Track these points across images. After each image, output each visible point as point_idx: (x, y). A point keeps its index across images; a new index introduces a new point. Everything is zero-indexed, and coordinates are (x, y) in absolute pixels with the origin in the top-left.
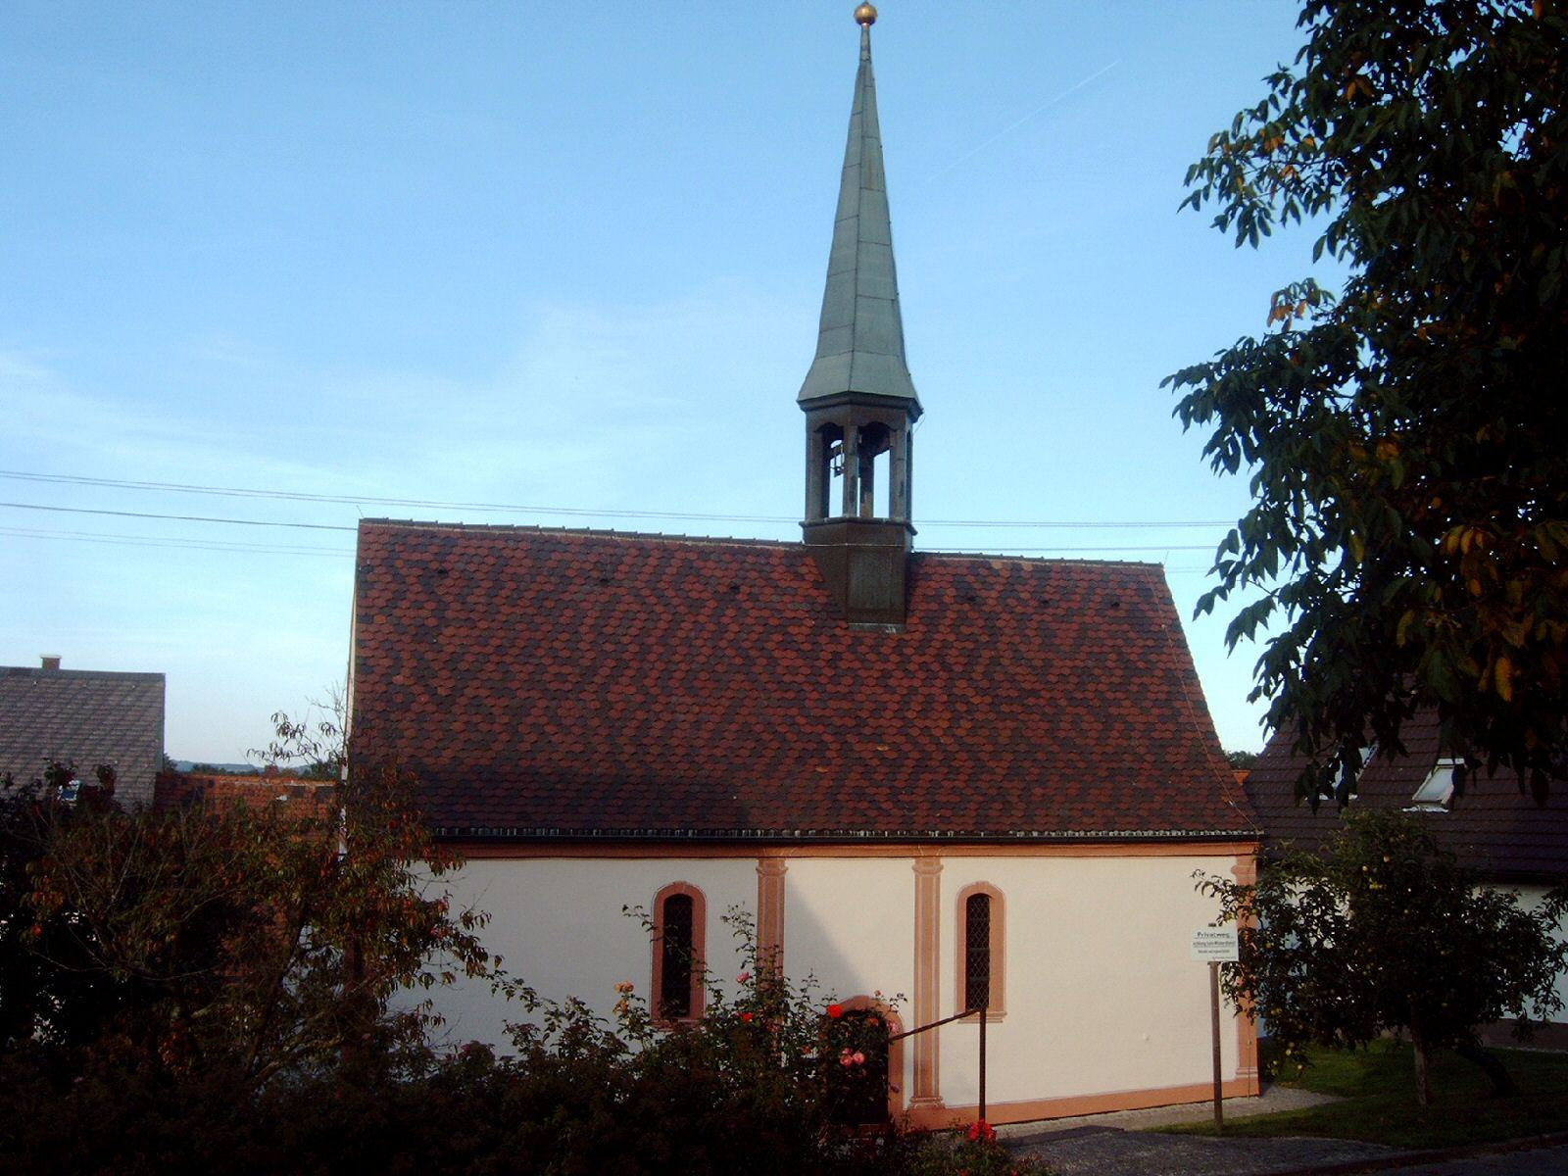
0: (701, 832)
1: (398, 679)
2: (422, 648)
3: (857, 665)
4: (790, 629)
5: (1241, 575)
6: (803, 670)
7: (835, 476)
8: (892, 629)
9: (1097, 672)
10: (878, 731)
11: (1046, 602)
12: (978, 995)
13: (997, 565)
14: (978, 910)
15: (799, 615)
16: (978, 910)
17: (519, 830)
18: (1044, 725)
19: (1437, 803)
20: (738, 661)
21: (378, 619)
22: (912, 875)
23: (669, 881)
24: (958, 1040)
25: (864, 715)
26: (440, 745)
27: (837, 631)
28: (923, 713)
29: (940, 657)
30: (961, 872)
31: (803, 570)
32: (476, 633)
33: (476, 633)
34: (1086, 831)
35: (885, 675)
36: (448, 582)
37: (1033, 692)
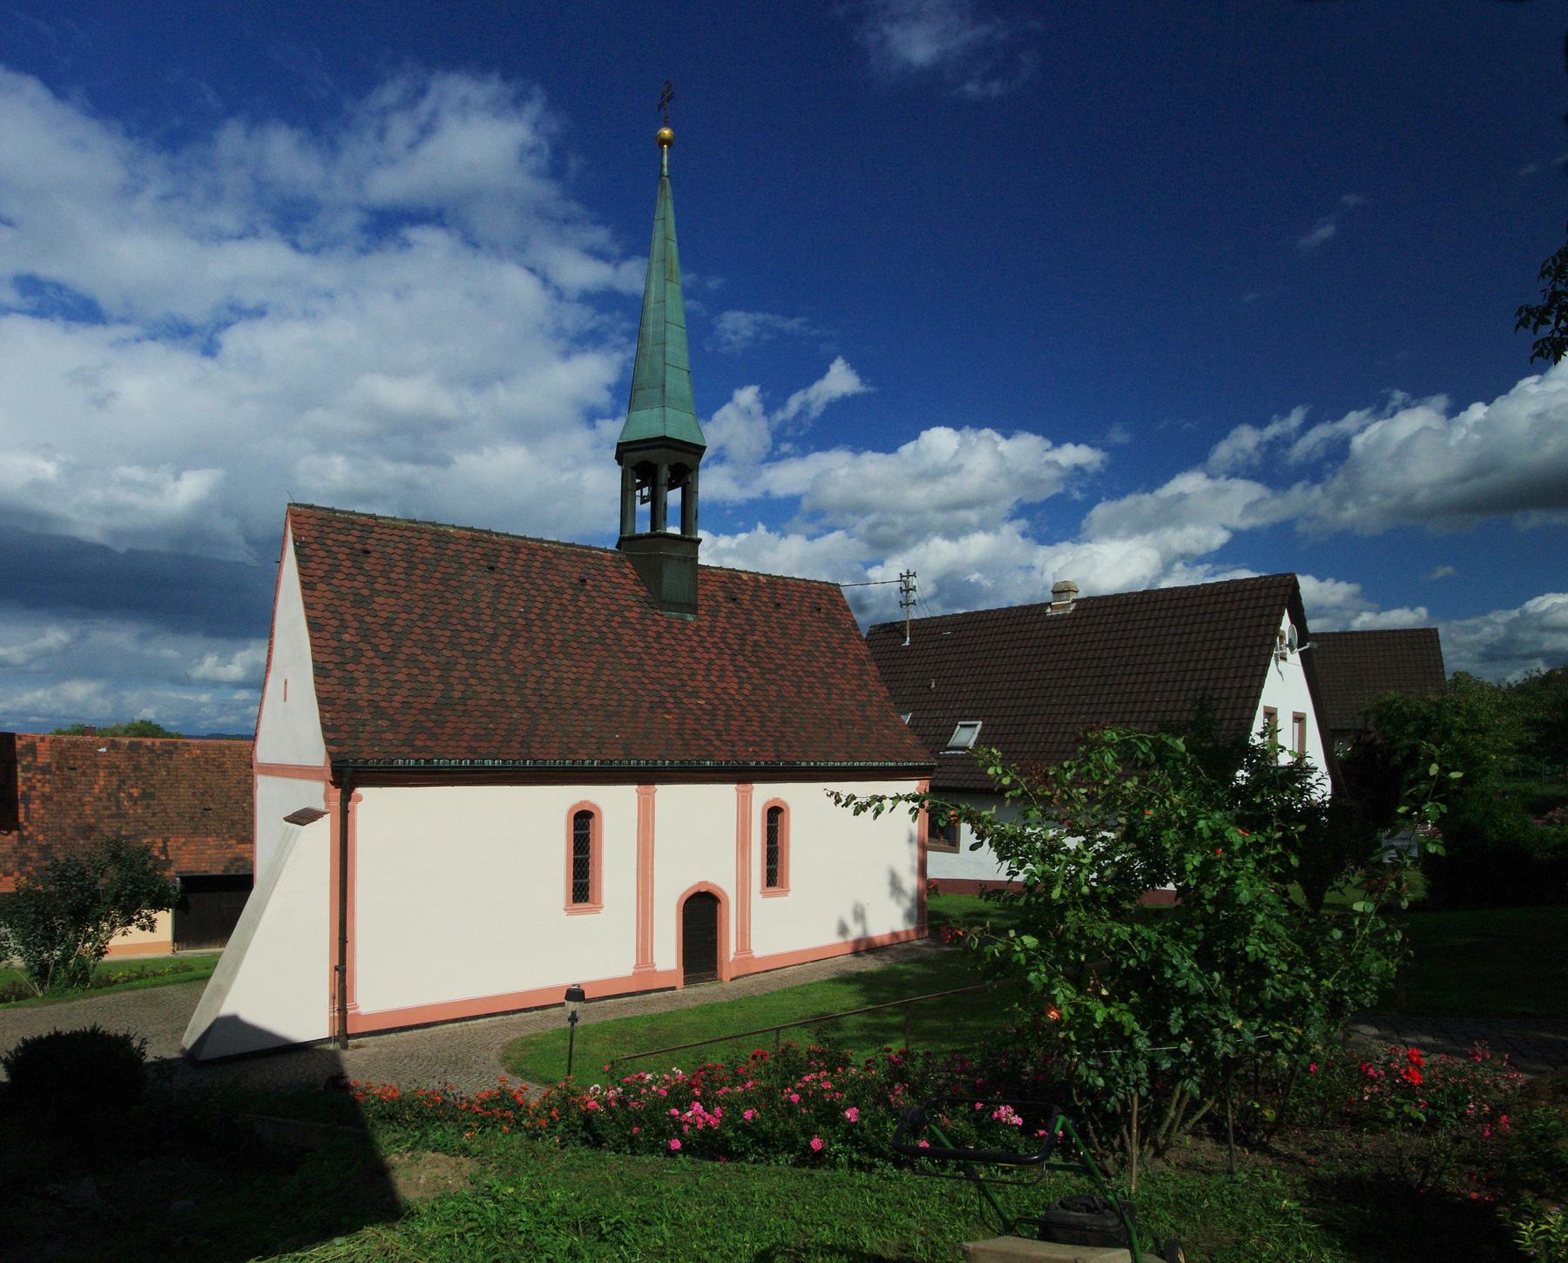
0: (602, 762)
1: (347, 637)
2: (362, 612)
3: (673, 642)
4: (626, 613)
5: (1377, 1032)
6: (640, 644)
7: (642, 503)
8: (690, 618)
9: (817, 654)
10: (695, 689)
11: (778, 605)
12: (774, 876)
13: (745, 577)
14: (775, 814)
15: (631, 604)
16: (775, 814)
17: (472, 761)
18: (795, 690)
19: (962, 726)
20: (596, 635)
21: (320, 586)
22: (636, 795)
23: (771, 797)
24: (764, 906)
25: (685, 677)
26: (391, 692)
27: (657, 617)
28: (721, 678)
29: (723, 639)
30: (764, 793)
31: (626, 571)
32: (402, 602)
33: (402, 602)
34: (841, 762)
35: (693, 650)
36: (371, 560)
37: (783, 667)
